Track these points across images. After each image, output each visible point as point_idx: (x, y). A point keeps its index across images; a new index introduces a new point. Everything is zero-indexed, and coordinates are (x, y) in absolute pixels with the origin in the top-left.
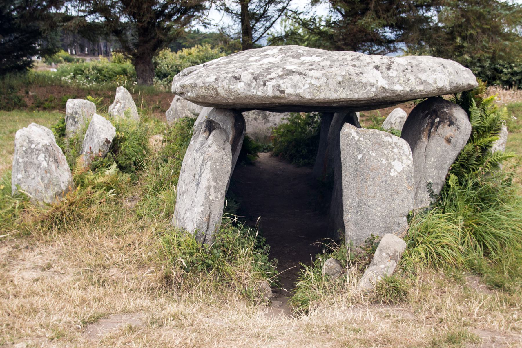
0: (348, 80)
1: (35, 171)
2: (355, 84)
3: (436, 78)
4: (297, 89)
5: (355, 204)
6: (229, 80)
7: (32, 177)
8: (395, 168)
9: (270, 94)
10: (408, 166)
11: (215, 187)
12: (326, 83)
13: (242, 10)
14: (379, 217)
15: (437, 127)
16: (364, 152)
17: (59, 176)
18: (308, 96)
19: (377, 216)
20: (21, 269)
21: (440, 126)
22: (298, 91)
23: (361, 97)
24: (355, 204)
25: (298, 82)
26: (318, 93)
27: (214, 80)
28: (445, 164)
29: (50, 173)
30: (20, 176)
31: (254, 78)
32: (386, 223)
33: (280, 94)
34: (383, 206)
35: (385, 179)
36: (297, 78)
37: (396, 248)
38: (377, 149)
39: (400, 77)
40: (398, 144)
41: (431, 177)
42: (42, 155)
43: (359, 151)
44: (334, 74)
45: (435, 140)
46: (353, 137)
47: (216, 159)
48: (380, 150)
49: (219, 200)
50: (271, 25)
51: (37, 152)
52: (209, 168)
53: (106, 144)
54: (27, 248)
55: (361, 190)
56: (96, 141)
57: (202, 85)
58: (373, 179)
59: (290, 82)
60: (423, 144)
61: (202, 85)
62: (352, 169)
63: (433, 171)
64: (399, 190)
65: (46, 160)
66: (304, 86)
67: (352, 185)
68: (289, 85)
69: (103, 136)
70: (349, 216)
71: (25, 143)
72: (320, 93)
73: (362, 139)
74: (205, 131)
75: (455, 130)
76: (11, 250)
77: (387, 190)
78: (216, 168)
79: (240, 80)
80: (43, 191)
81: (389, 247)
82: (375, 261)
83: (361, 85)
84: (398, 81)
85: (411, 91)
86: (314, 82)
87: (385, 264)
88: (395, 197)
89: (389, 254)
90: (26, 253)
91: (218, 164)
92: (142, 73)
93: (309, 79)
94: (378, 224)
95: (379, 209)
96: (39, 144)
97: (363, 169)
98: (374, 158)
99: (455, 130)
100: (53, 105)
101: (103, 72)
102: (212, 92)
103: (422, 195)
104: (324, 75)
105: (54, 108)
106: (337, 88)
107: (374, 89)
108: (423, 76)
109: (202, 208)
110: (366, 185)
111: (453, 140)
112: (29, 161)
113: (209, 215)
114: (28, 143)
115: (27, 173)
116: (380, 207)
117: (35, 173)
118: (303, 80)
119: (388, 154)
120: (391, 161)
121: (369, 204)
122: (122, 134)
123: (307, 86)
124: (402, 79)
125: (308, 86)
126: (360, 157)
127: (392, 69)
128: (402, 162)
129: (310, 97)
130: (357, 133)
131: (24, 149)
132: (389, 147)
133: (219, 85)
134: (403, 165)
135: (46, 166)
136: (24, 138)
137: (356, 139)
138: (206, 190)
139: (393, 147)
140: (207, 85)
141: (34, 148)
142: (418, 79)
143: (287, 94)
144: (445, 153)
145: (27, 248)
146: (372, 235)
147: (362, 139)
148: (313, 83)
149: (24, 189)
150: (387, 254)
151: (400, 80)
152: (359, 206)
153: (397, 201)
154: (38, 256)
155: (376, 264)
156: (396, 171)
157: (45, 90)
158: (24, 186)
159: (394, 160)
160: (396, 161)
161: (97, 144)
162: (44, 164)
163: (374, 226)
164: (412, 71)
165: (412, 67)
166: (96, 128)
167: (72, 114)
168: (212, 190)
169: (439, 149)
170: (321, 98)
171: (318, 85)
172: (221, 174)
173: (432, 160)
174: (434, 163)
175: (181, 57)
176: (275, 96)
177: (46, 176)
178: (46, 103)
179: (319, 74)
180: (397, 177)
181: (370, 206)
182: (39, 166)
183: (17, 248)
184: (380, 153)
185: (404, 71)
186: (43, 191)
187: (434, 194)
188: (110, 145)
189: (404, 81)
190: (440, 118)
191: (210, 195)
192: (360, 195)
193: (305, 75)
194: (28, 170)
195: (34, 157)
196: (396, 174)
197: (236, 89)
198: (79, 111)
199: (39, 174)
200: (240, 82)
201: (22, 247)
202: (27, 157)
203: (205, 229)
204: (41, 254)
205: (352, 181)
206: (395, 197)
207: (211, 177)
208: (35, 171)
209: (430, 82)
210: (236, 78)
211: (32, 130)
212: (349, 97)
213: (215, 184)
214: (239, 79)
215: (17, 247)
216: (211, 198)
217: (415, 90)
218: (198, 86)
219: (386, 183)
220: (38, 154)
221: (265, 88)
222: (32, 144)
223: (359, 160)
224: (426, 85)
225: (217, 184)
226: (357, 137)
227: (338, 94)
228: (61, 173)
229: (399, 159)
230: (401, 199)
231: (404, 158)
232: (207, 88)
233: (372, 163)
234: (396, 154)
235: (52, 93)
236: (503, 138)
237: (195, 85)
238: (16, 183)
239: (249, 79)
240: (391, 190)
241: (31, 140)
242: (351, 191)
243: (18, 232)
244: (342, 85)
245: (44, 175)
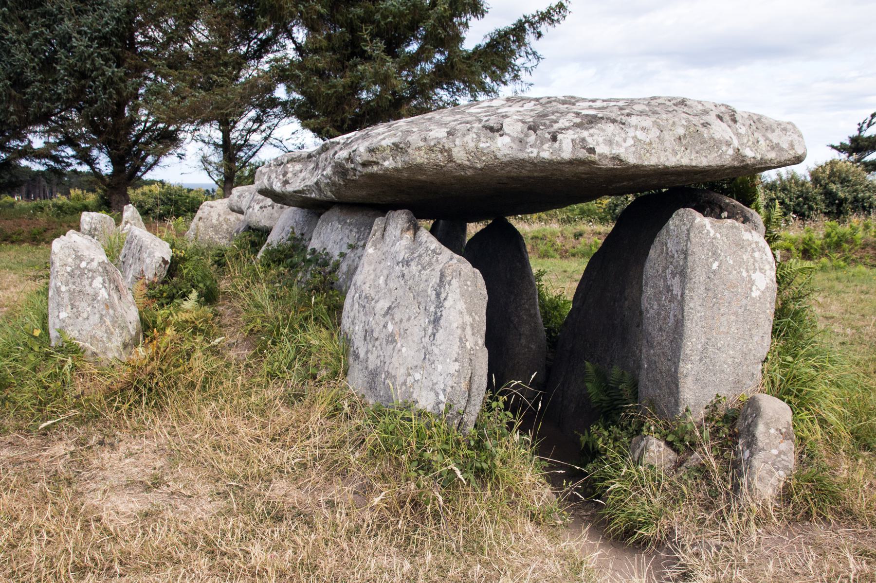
0: (694, 134)
1: (89, 305)
2: (704, 142)
3: (792, 141)
4: (614, 146)
5: (699, 347)
6: (478, 134)
7: (85, 315)
9: (567, 153)
11: (472, 325)
12: (659, 137)
13: (224, 137)
14: (729, 366)
17: (124, 313)
18: (632, 160)
19: (727, 364)
20: (105, 491)
22: (616, 151)
24: (699, 347)
25: (615, 136)
26: (648, 155)
27: (446, 135)
29: (113, 308)
30: (63, 315)
31: (530, 128)
32: (738, 375)
33: (587, 154)
34: (738, 348)
35: (744, 302)
40: (760, 245)
43: (715, 255)
44: (671, 122)
46: (708, 232)
50: (254, 154)
51: (90, 274)
52: (458, 290)
53: (163, 266)
54: (101, 443)
55: (711, 322)
56: (148, 261)
57: (422, 144)
58: (730, 303)
59: (602, 134)
61: (422, 144)
62: (703, 288)
64: (760, 320)
65: (105, 287)
66: (625, 141)
67: (699, 315)
68: (601, 140)
69: (158, 255)
70: (689, 366)
71: (70, 260)
72: (651, 154)
73: (718, 235)
74: (408, 229)
76: (72, 448)
78: (467, 290)
79: (502, 132)
80: (105, 339)
81: (779, 419)
82: (760, 444)
83: (712, 143)
85: (761, 159)
86: (640, 135)
87: (776, 448)
89: (780, 430)
90: (103, 455)
91: (469, 283)
92: (117, 204)
93: (632, 129)
94: (727, 377)
95: (731, 352)
96: (92, 260)
97: (718, 287)
98: (732, 268)
100: (22, 238)
101: (64, 209)
102: (440, 156)
105: (23, 241)
106: (676, 148)
108: (774, 137)
109: (457, 366)
110: (719, 313)
112: (78, 289)
114: (74, 259)
115: (75, 310)
116: (734, 349)
117: (89, 309)
118: (622, 132)
122: (181, 252)
123: (630, 142)
125: (632, 142)
126: (715, 266)
128: (764, 273)
129: (635, 161)
130: (713, 226)
131: (69, 269)
133: (457, 143)
135: (107, 297)
136: (67, 251)
137: (711, 235)
138: (459, 331)
140: (432, 143)
141: (86, 268)
142: (768, 141)
143: (599, 155)
145: (101, 443)
146: (718, 396)
147: (718, 235)
148: (639, 137)
149: (72, 333)
150: (777, 430)
151: (749, 140)
152: (705, 349)
153: (755, 339)
154: (127, 461)
155: (763, 449)
156: (759, 290)
157: (12, 222)
158: (72, 331)
160: (758, 272)
161: (150, 266)
162: (103, 294)
163: (721, 382)
166: (146, 243)
167: (90, 231)
168: (468, 329)
170: (652, 163)
171: (648, 141)
175: (144, 194)
176: (576, 160)
177: (108, 313)
178: (14, 237)
179: (647, 122)
180: (760, 298)
182: (95, 297)
183: (83, 445)
184: (738, 259)
188: (168, 266)
191: (467, 341)
192: (709, 330)
193: (624, 124)
194: (77, 304)
195: (86, 282)
197: (492, 148)
198: (98, 226)
199: (96, 311)
200: (501, 135)
201: (93, 440)
202: (74, 283)
203: (463, 403)
204: (131, 455)
205: (699, 308)
206: (754, 331)
207: (464, 306)
208: (89, 305)
210: (492, 129)
211: (72, 240)
212: (694, 164)
214: (498, 131)
215: (81, 443)
216: (468, 345)
218: (413, 146)
219: (745, 309)
220: (93, 278)
221: (557, 145)
222: (81, 261)
223: (714, 272)
225: (473, 321)
226: (712, 232)
227: (678, 157)
228: (126, 309)
229: (761, 269)
230: (761, 335)
232: (431, 149)
233: (731, 276)
234: (757, 261)
235: (20, 226)
237: (406, 144)
238: (58, 327)
239: (520, 129)
241: (79, 254)
243: (78, 413)
244: (684, 142)
245: (104, 313)
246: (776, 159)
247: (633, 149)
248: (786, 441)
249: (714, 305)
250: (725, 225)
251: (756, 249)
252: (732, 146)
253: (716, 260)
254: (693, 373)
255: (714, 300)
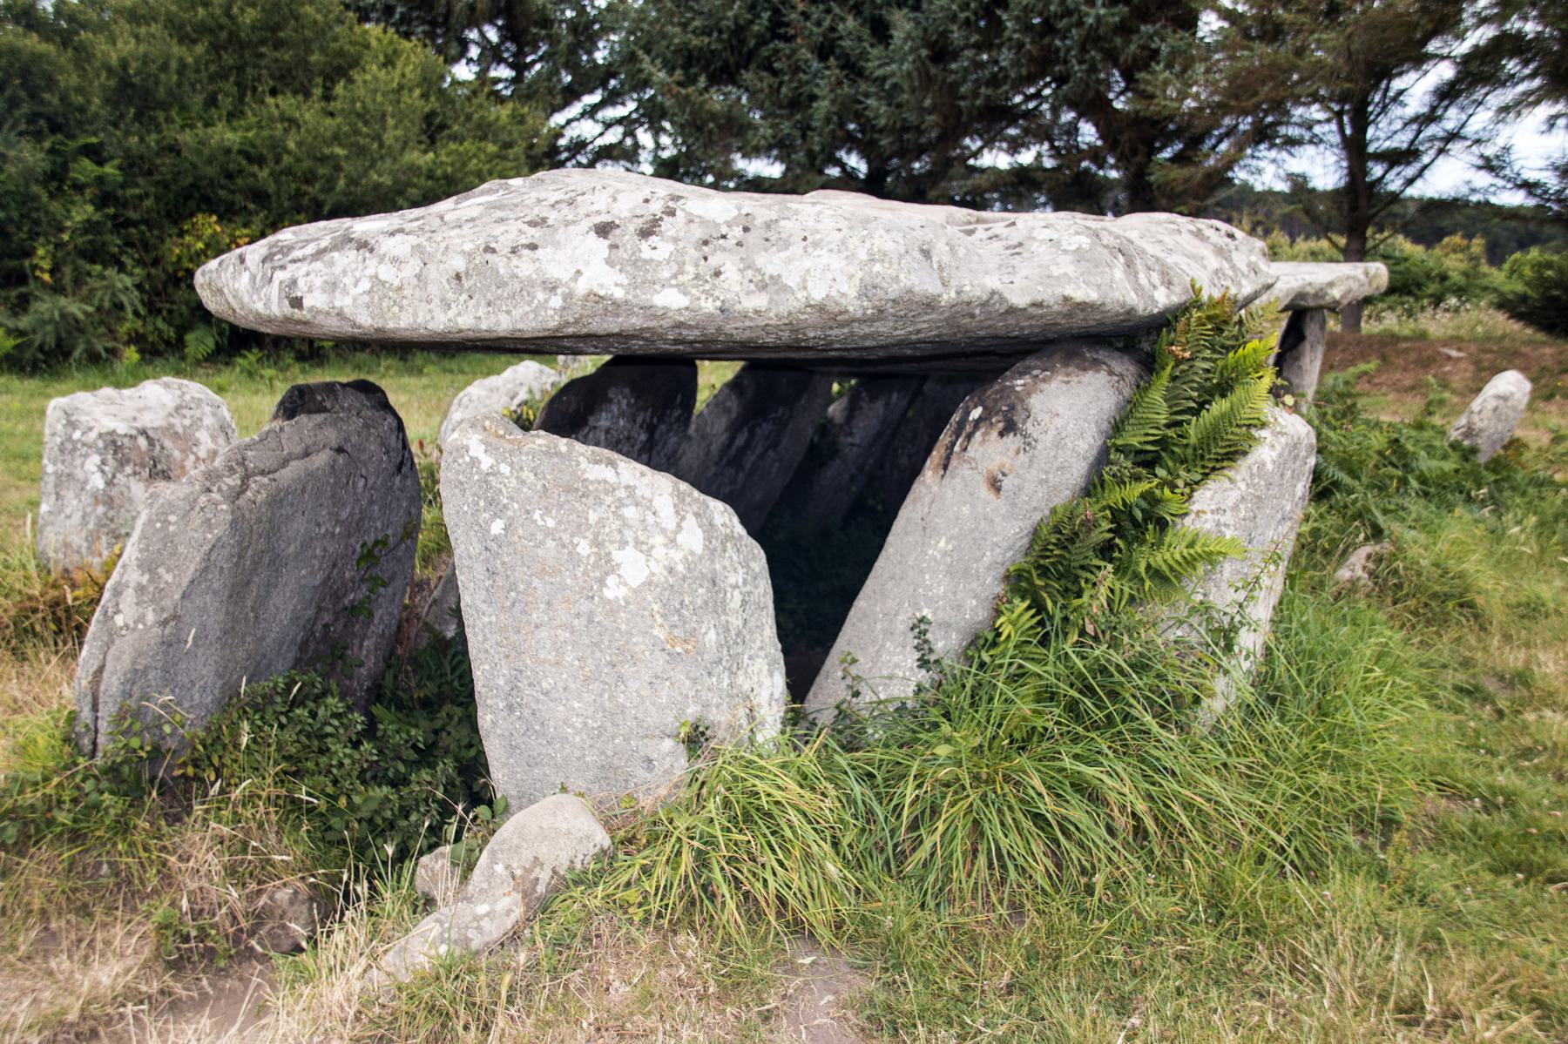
4: (337, 294)
5: (501, 682)
8: (621, 572)
10: (671, 570)
11: (141, 589)
12: (418, 276)
15: (969, 437)
16: (510, 513)
19: (574, 727)
21: (978, 435)
23: (520, 326)
24: (501, 682)
25: (345, 272)
26: (396, 309)
28: (977, 561)
32: (603, 753)
35: (585, 606)
36: (346, 261)
37: (543, 852)
38: (561, 506)
39: (681, 264)
40: (639, 493)
41: (930, 601)
42: (96, 459)
45: (958, 480)
46: (475, 462)
47: (169, 503)
48: (573, 510)
49: (147, 629)
50: (1420, 174)
55: (514, 637)
60: (923, 489)
62: (480, 569)
63: (939, 584)
65: (103, 472)
66: (356, 285)
68: (318, 282)
71: (60, 427)
72: (401, 308)
73: (505, 469)
75: (1018, 452)
77: (596, 645)
80: (84, 550)
83: (517, 286)
84: (675, 276)
86: (387, 272)
88: (627, 670)
91: (172, 518)
94: (578, 753)
95: (576, 705)
96: (90, 429)
98: (546, 535)
99: (1018, 452)
103: (896, 659)
104: (417, 249)
106: (450, 295)
107: (556, 302)
108: (770, 263)
111: (1006, 483)
113: (101, 670)
114: (65, 426)
116: (580, 699)
119: (601, 523)
120: (612, 548)
121: (544, 684)
123: (365, 285)
124: (690, 269)
126: (497, 527)
127: (660, 234)
129: (370, 321)
132: (609, 500)
134: (652, 564)
137: (485, 467)
139: (620, 499)
142: (750, 273)
143: (311, 309)
144: (983, 524)
147: (505, 469)
148: (382, 277)
151: (681, 272)
153: (633, 685)
156: (626, 584)
159: (623, 544)
160: (630, 549)
164: (739, 244)
165: (746, 229)
169: (966, 510)
170: (403, 324)
171: (397, 283)
172: (181, 549)
173: (942, 544)
174: (945, 554)
180: (627, 603)
181: (547, 694)
185: (706, 243)
186: (84, 550)
187: (932, 658)
189: (697, 277)
190: (985, 408)
191: (118, 612)
192: (513, 654)
195: (78, 462)
196: (622, 592)
202: (63, 462)
205: (484, 607)
206: (627, 670)
209: (789, 283)
212: (484, 327)
213: (145, 579)
216: (119, 620)
217: (738, 307)
219: (590, 621)
220: (86, 456)
223: (495, 539)
224: (777, 293)
225: (151, 581)
226: (486, 462)
227: (451, 314)
229: (638, 543)
231: (658, 540)
233: (540, 552)
234: (631, 527)
236: (1242, 486)
240: (609, 647)
242: (485, 639)
244: (467, 284)
246: (769, 310)
247: (366, 298)
248: (514, 895)
249: (513, 604)
250: (525, 449)
251: (627, 502)
252: (559, 291)
253: (496, 516)
254: (499, 732)
255: (513, 594)
